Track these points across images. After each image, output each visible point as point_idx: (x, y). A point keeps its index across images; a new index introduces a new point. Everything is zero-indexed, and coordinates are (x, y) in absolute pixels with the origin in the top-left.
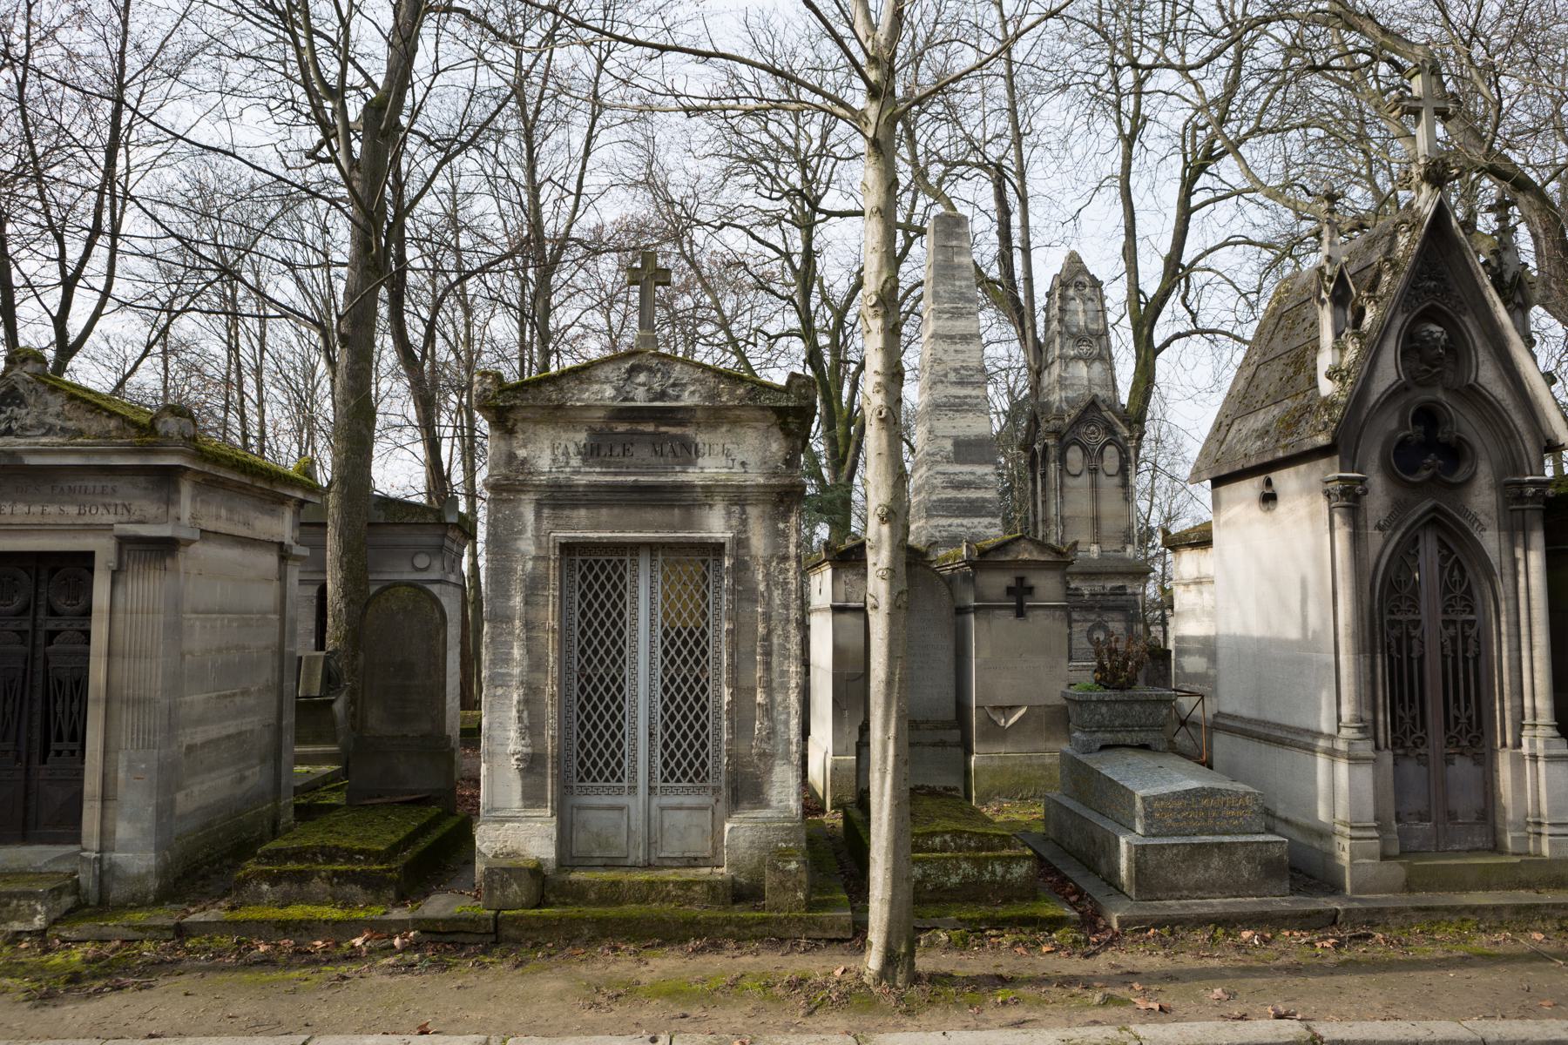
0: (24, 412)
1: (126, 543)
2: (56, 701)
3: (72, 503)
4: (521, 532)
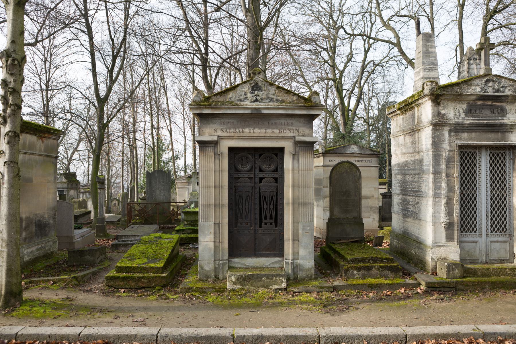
0: (261, 93)
1: (298, 144)
3: (276, 128)
4: (443, 141)
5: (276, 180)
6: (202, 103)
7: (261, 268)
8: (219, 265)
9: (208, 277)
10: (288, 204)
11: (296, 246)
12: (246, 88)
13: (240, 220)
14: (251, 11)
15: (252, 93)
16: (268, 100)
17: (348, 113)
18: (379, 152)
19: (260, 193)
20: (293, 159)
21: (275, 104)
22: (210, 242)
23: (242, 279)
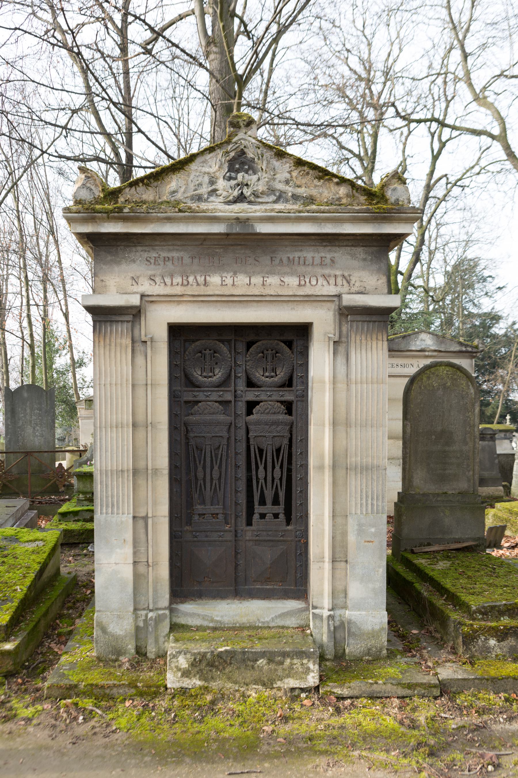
0: (255, 178)
1: (349, 314)
2: (257, 468)
3: (292, 274)
5: (289, 407)
6: (98, 207)
7: (253, 629)
8: (145, 621)
9: (119, 652)
10: (321, 468)
11: (339, 573)
12: (215, 164)
13: (199, 508)
14: (218, 40)
15: (230, 178)
16: (273, 198)
17: (396, 277)
18: (477, 347)
19: (248, 439)
20: (334, 353)
21: (289, 206)
22: (125, 561)
23: (204, 664)
